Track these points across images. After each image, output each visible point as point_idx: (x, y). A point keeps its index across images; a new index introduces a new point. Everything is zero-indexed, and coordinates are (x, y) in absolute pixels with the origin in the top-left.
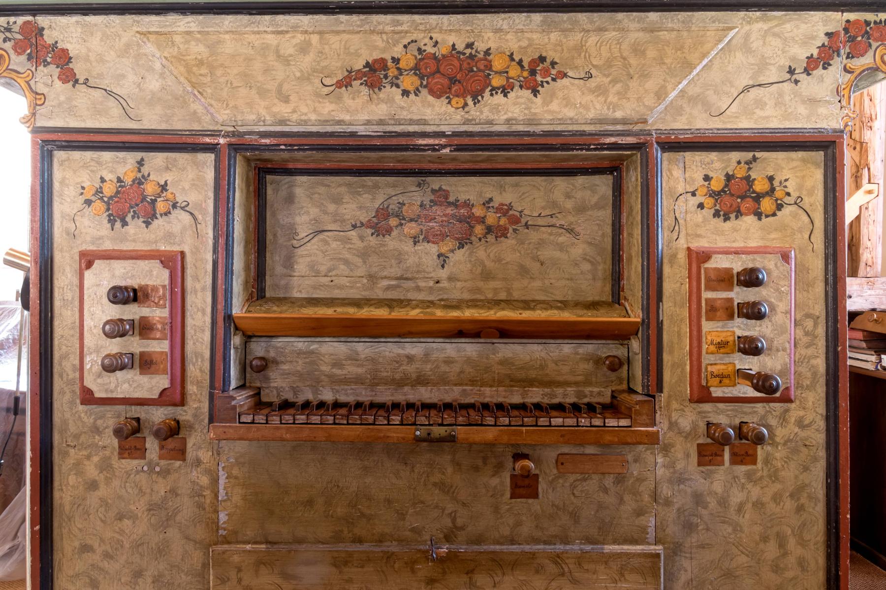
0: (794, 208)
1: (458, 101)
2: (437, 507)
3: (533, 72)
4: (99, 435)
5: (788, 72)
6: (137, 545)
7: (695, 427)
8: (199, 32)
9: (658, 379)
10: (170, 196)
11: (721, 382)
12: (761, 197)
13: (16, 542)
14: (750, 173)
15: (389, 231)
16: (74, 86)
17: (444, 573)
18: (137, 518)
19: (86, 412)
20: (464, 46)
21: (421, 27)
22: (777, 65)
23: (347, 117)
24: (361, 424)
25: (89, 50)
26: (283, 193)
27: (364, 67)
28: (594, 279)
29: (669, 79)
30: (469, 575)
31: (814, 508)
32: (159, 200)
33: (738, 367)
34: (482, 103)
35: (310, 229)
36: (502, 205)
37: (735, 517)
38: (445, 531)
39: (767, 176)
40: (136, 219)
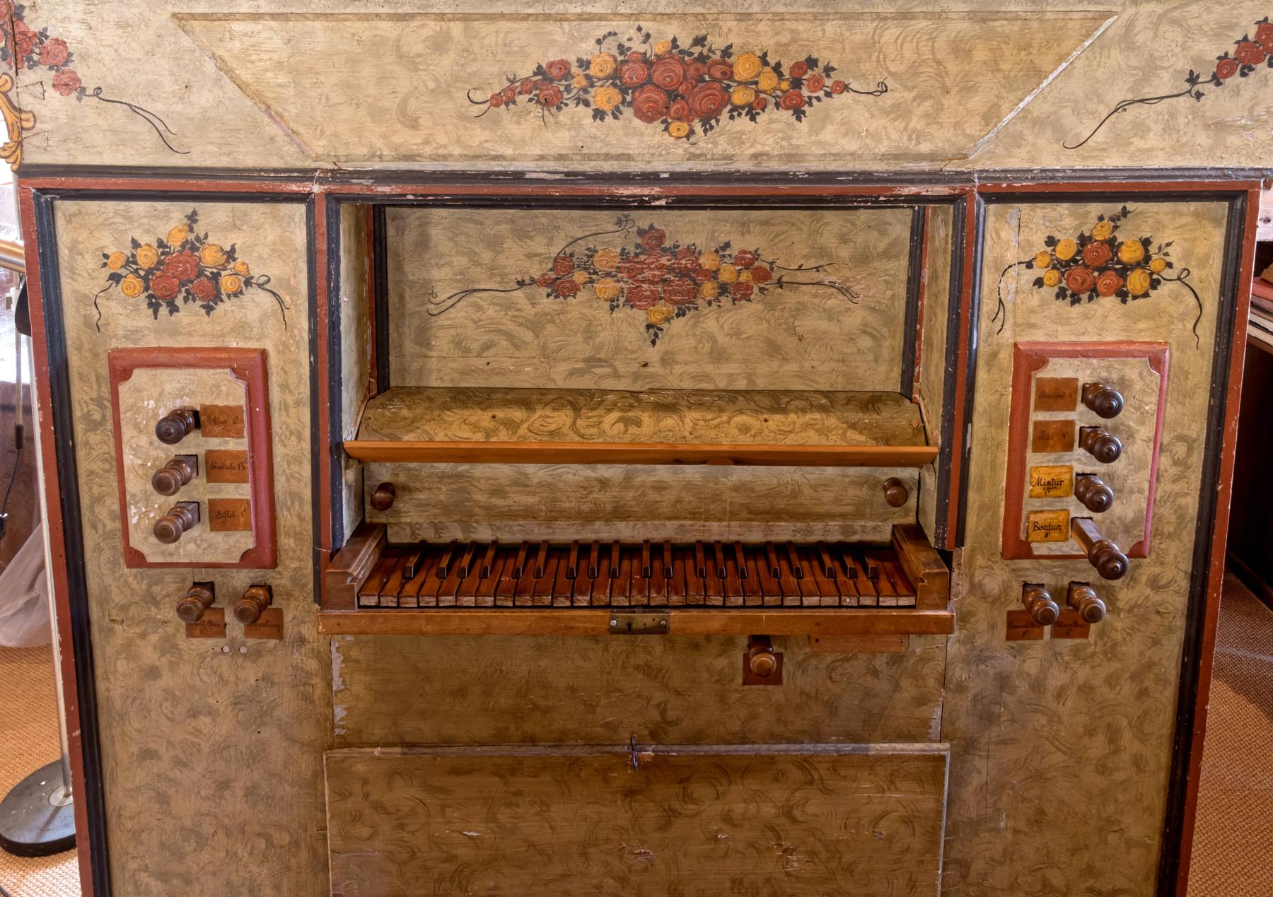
0: (1175, 286)
1: (680, 127)
2: (639, 696)
4: (156, 607)
5: (1188, 81)
6: (221, 749)
7: (1005, 589)
9: (958, 517)
10: (240, 268)
11: (1046, 535)
12: (1128, 270)
13: (34, 594)
14: (1116, 234)
15: (574, 290)
16: (79, 99)
17: (649, 782)
18: (218, 715)
19: (135, 576)
20: (690, 41)
22: (1172, 69)
23: (509, 152)
24: (533, 607)
27: (535, 74)
28: (876, 360)
29: (1005, 95)
30: (683, 785)
31: (1161, 693)
32: (223, 273)
33: (1073, 515)
34: (717, 129)
35: (453, 288)
36: (744, 252)
37: (1052, 705)
38: (651, 726)
39: (1140, 239)
40: (191, 301)
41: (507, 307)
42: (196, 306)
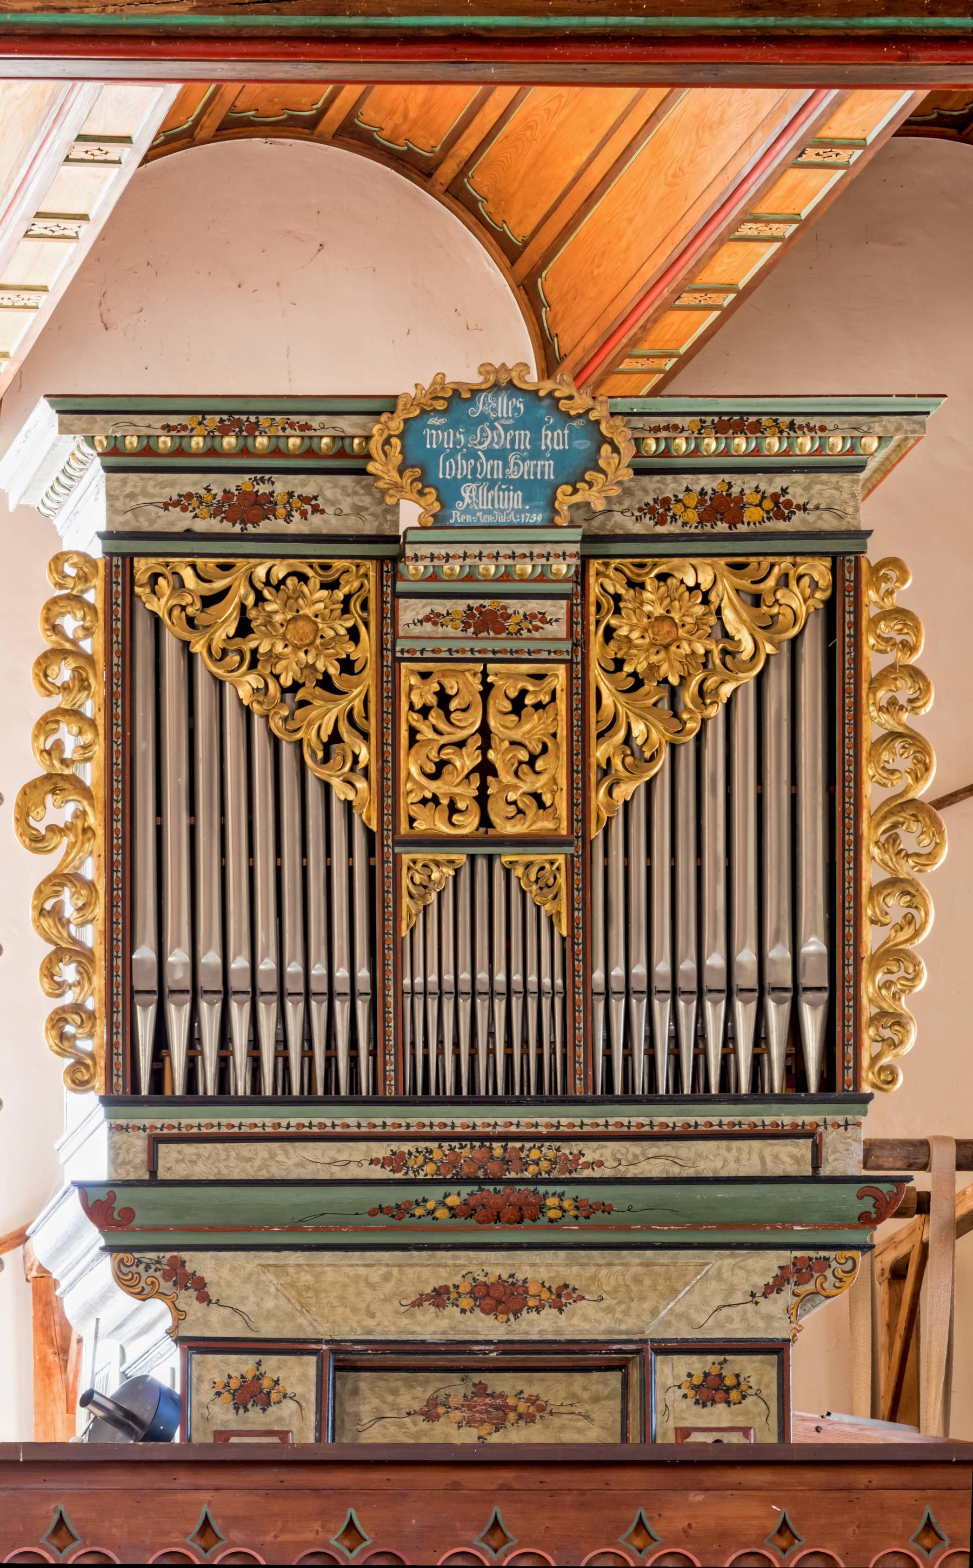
1: (503, 1317)
3: (559, 1296)
8: (307, 1265)
10: (282, 1389)
15: (437, 1417)
21: (475, 1262)
23: (418, 1329)
25: (220, 1278)
26: (349, 1386)
41: (402, 1426)
42: (258, 1409)
